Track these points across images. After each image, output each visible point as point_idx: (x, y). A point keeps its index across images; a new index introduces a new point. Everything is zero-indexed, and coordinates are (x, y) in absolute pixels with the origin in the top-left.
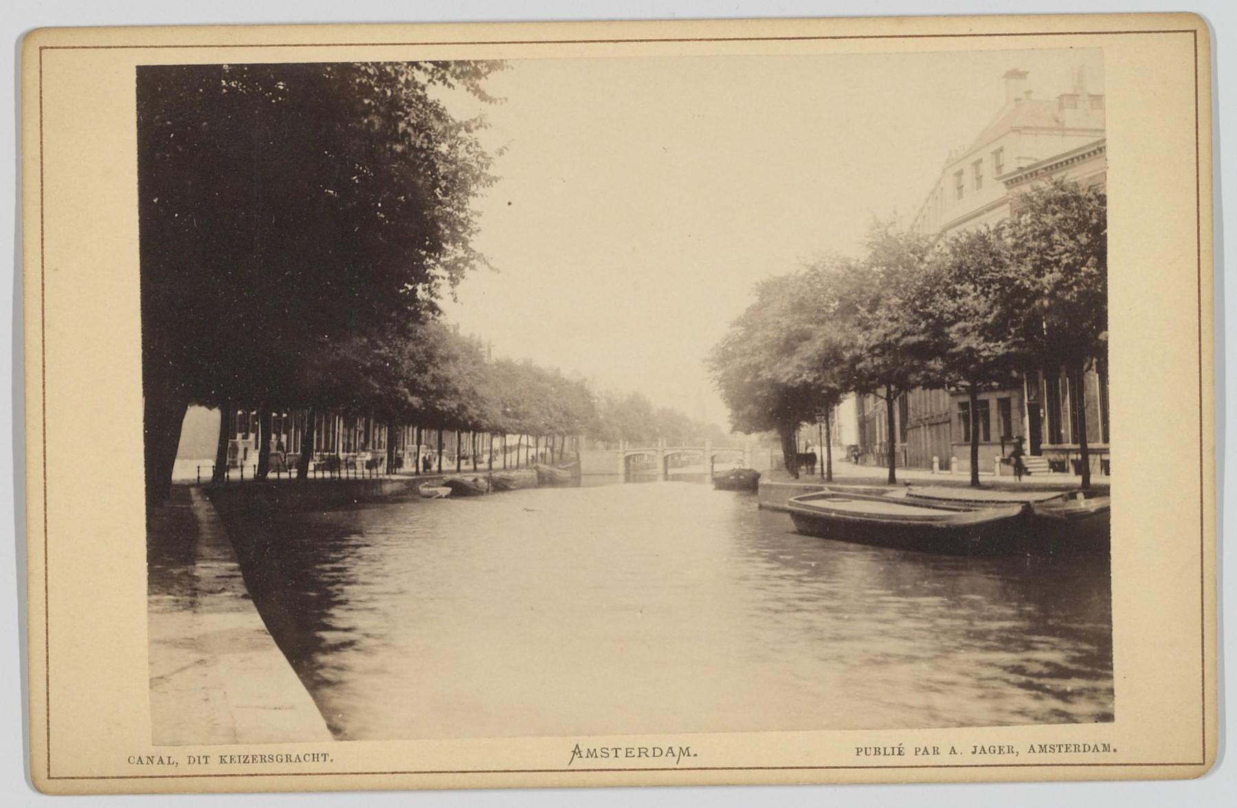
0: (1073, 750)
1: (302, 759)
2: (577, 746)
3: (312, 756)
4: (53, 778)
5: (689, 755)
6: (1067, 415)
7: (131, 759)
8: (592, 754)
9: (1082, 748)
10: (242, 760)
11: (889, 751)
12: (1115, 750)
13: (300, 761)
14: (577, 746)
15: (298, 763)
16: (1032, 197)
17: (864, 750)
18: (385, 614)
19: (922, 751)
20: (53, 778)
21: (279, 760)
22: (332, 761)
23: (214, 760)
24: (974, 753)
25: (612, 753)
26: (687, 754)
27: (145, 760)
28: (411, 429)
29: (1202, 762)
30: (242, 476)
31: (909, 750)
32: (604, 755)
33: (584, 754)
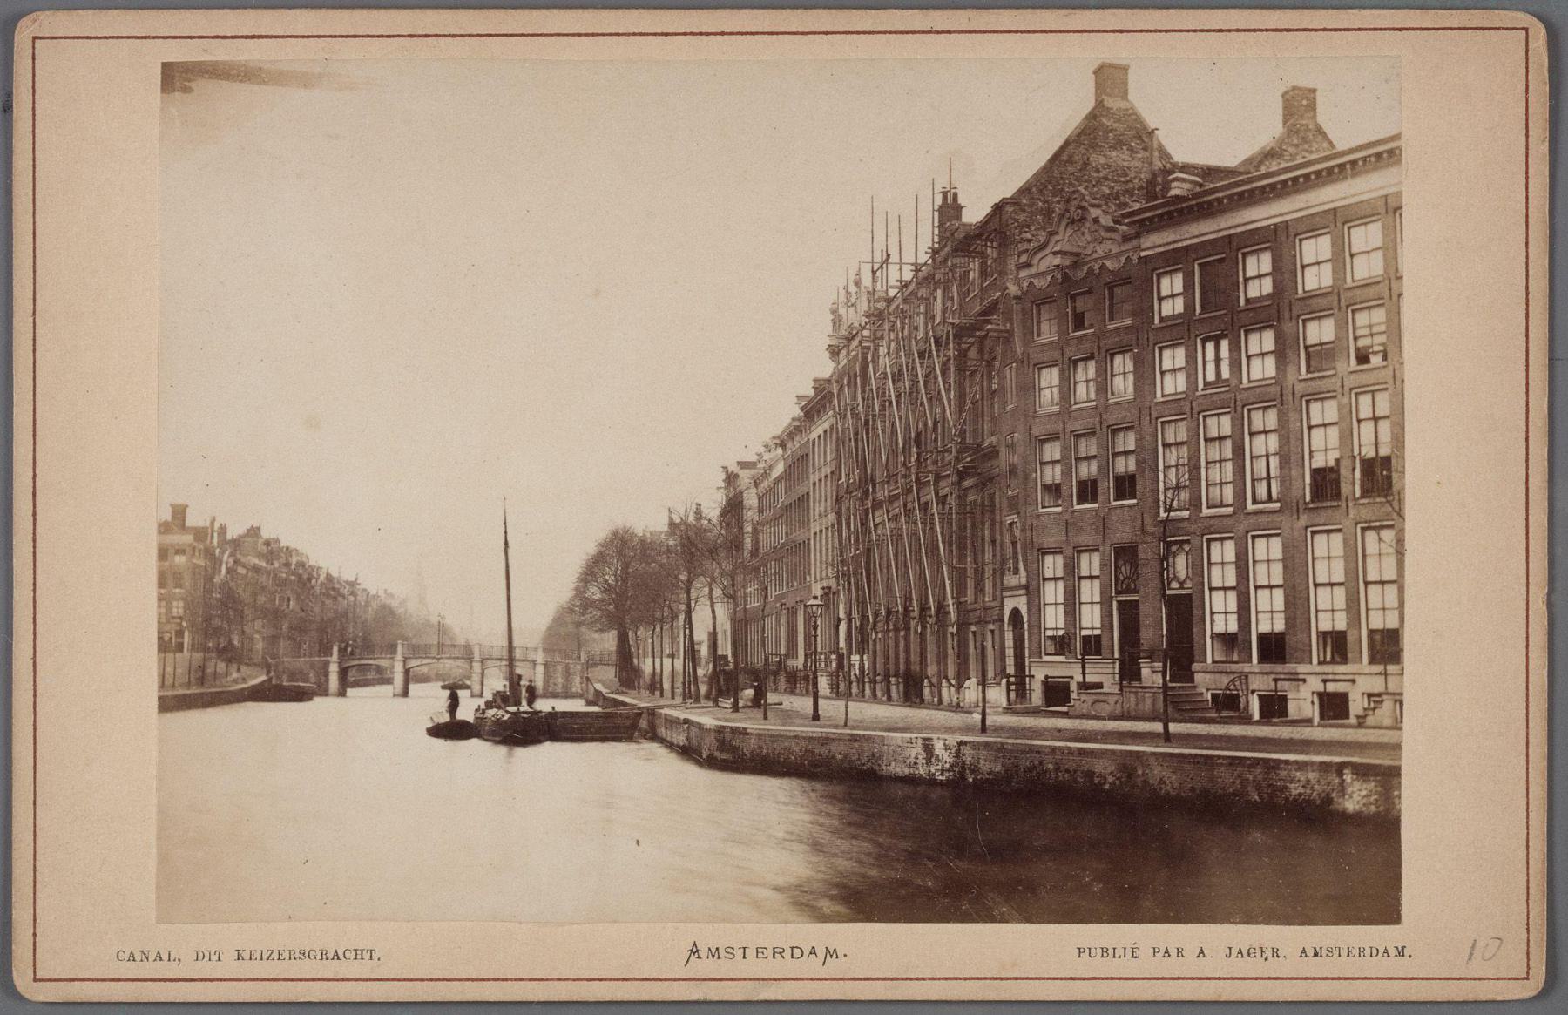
0: (364, 952)
1: (341, 956)
2: (695, 945)
3: (353, 952)
4: (1528, 973)
5: (719, 958)
6: (931, 577)
7: (121, 954)
8: (715, 953)
9: (1367, 952)
10: (265, 956)
11: (1120, 952)
12: (1410, 956)
13: (338, 959)
14: (695, 945)
15: (336, 961)
16: (1053, 212)
17: (1087, 950)
18: (340, 567)
19: (1161, 953)
20: (1528, 973)
21: (312, 957)
22: (845, 956)
23: (229, 956)
24: (1228, 956)
25: (739, 953)
26: (716, 956)
27: (138, 956)
28: (1210, 346)
29: (37, 977)
30: (1271, 352)
31: (1145, 952)
32: (727, 955)
33: (703, 953)
